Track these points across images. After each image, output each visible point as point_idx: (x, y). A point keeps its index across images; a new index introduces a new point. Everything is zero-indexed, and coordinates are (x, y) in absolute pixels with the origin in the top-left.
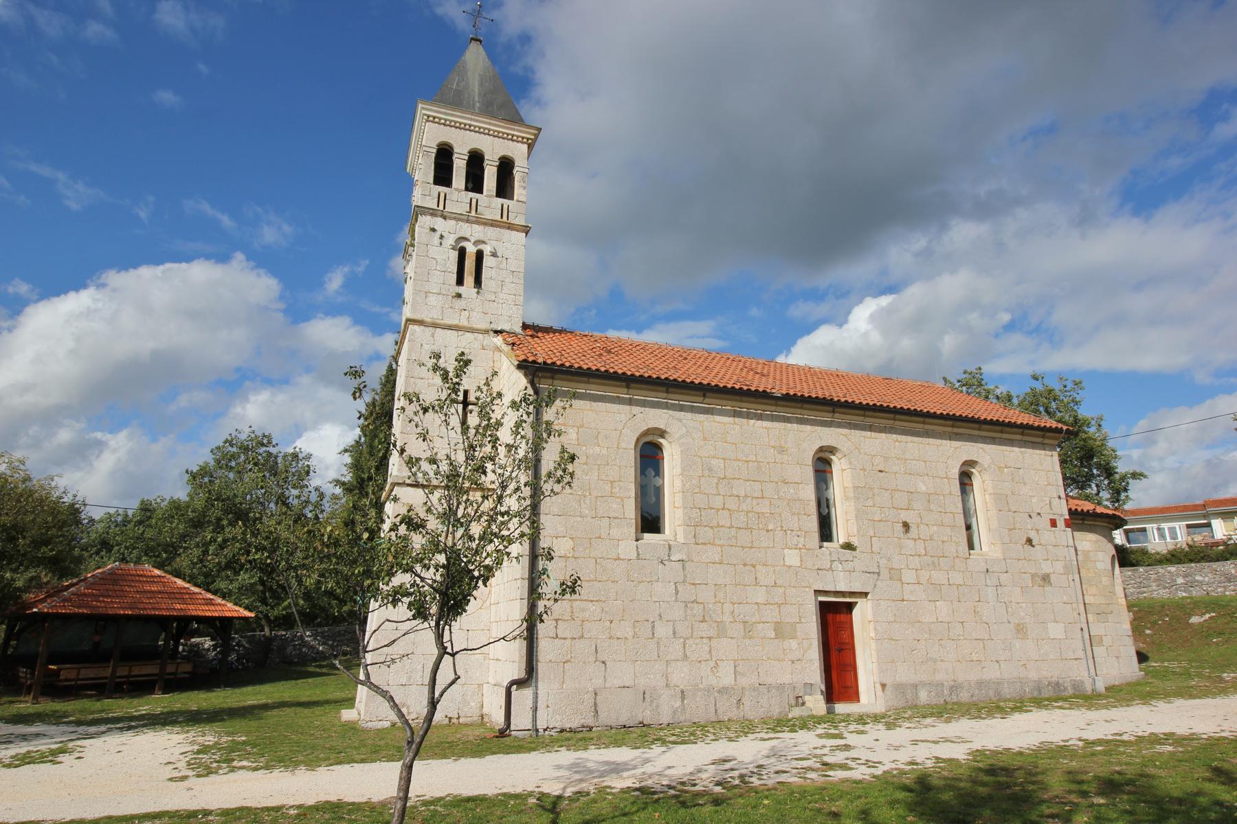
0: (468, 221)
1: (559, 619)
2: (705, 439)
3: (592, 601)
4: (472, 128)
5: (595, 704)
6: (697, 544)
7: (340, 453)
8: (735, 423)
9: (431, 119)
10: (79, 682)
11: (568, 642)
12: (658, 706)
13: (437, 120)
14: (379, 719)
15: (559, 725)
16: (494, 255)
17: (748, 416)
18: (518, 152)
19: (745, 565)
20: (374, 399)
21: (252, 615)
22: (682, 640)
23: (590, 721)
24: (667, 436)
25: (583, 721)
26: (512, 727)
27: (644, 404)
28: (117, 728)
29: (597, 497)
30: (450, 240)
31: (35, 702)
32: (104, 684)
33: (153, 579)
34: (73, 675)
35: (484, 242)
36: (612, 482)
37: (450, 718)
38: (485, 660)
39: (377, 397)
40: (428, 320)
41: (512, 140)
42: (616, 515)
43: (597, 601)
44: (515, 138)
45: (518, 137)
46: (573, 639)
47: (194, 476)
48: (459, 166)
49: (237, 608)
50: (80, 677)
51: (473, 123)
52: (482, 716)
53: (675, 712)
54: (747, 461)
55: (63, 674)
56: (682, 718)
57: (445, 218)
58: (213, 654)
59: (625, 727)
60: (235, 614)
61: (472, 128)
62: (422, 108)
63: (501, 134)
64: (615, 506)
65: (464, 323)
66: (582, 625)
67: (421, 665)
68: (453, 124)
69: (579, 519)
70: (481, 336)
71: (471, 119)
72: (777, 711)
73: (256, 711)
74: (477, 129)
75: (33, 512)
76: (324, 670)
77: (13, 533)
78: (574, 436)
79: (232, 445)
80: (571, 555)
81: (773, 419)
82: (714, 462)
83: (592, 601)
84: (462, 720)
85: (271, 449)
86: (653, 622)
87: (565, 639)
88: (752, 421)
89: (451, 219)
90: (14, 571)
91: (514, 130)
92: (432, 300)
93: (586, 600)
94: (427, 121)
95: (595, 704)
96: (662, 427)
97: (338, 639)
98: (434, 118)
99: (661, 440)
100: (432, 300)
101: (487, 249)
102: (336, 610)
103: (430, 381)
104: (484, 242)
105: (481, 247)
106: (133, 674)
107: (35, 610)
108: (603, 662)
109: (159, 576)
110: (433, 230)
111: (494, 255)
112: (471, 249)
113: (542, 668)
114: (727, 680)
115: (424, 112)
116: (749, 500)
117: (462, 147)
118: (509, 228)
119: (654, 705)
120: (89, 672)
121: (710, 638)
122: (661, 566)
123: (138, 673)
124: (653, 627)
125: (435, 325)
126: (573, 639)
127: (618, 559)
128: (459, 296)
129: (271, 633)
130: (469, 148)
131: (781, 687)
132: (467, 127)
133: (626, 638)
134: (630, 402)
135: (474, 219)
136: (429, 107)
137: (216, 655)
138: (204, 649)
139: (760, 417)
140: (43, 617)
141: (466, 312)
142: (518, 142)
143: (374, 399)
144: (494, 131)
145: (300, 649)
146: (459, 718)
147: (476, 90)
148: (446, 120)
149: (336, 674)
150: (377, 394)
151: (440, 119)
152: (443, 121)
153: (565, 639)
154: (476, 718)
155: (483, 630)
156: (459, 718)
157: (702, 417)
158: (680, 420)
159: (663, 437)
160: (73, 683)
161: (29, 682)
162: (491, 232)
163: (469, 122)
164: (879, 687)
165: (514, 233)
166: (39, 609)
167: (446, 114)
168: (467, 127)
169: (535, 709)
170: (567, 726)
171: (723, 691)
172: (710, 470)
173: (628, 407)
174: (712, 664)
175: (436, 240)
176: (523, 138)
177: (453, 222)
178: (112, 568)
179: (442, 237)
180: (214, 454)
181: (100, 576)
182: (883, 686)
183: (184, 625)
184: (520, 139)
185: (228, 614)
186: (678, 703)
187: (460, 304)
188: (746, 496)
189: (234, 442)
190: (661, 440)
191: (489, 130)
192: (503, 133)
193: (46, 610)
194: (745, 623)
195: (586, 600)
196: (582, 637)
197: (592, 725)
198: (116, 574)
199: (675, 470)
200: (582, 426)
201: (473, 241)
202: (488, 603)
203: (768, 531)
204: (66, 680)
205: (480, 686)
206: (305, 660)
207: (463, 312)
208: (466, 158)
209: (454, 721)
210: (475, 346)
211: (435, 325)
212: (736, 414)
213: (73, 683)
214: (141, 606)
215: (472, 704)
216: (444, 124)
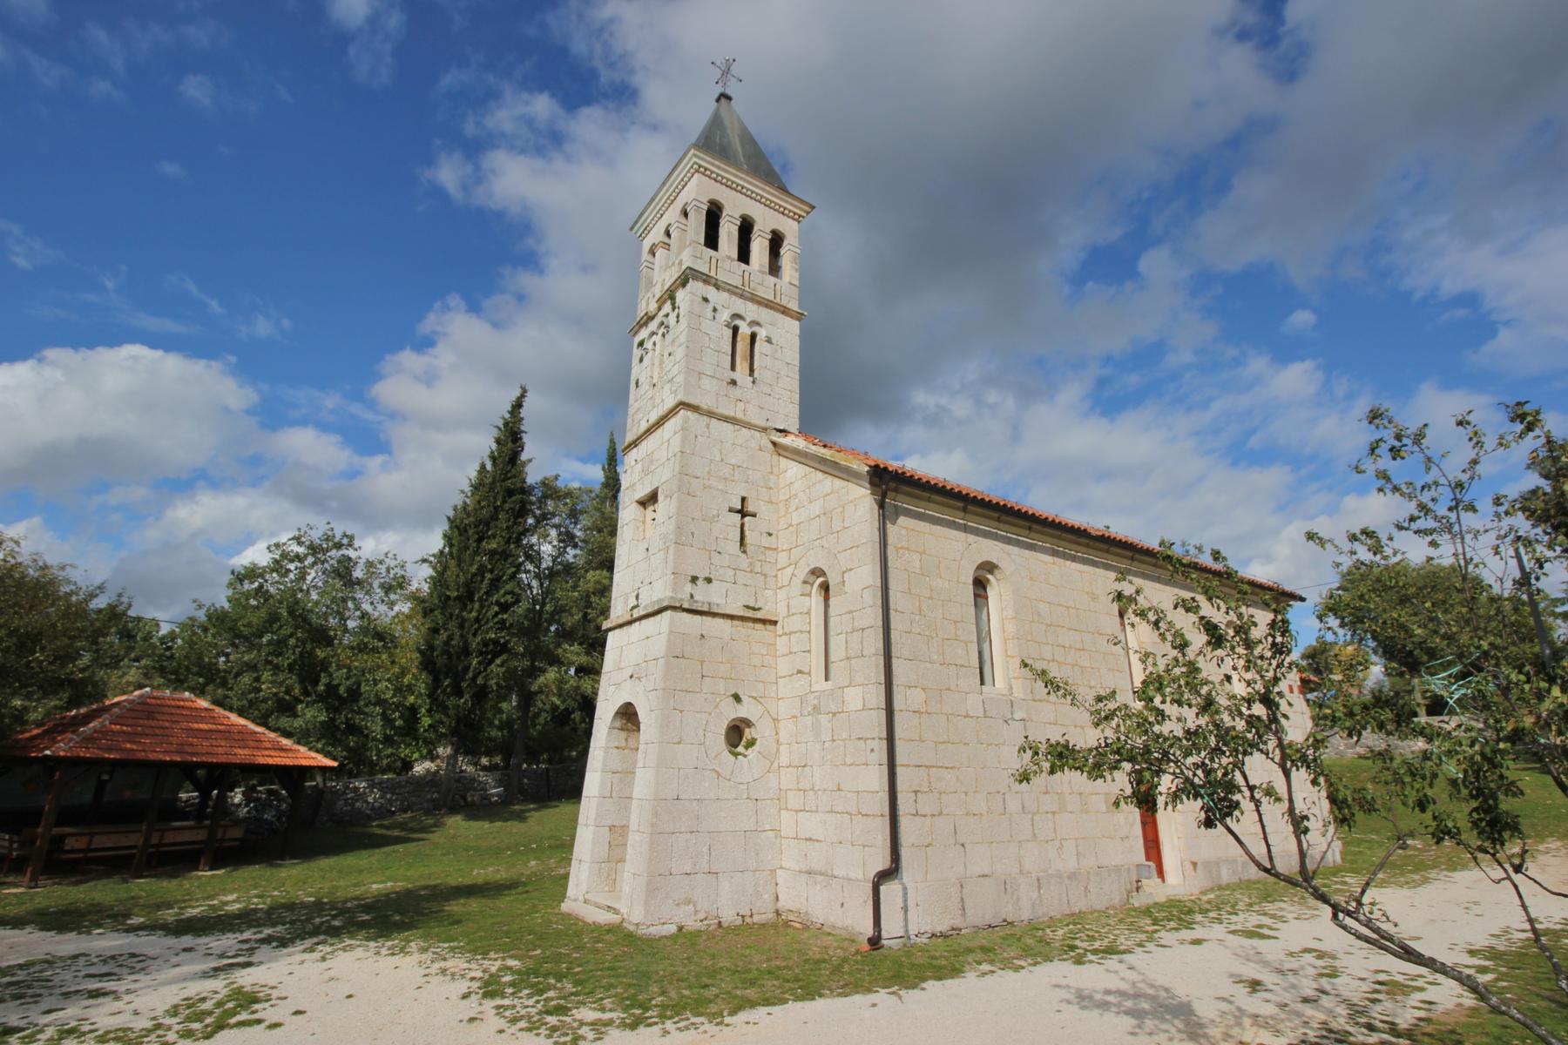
0: (741, 296)
1: (919, 791)
2: (1031, 579)
3: (947, 768)
4: (744, 190)
5: (962, 899)
6: (1034, 700)
7: (416, 562)
8: (1054, 563)
9: (702, 169)
10: (90, 854)
11: (928, 819)
12: (1018, 899)
13: (708, 173)
14: (662, 921)
15: (929, 928)
16: (769, 341)
17: (1064, 556)
18: (789, 228)
19: (1076, 726)
20: (465, 503)
21: (335, 764)
22: (1030, 816)
23: (958, 922)
24: (996, 572)
25: (952, 921)
26: (884, 934)
27: (977, 532)
28: (267, 941)
29: (943, 639)
30: (725, 316)
31: (33, 884)
32: (132, 857)
33: (197, 714)
34: (81, 843)
35: (758, 324)
36: (956, 622)
37: (743, 916)
38: (776, 838)
39: (468, 501)
40: (704, 406)
41: (783, 213)
42: (962, 663)
43: (952, 768)
44: (786, 212)
45: (790, 211)
46: (933, 815)
47: (1344, 576)
48: (728, 232)
49: (313, 754)
50: (93, 847)
51: (746, 185)
52: (778, 913)
53: (1033, 905)
54: (1068, 608)
55: (70, 843)
56: (1040, 913)
57: (718, 289)
58: (246, 809)
59: (990, 926)
60: (313, 763)
61: (744, 190)
62: (695, 155)
63: (773, 205)
64: (960, 651)
65: (740, 415)
66: (939, 799)
67: (707, 847)
68: (724, 181)
69: (928, 665)
70: (758, 434)
71: (745, 180)
72: (1118, 898)
73: (455, 907)
74: (749, 193)
75: (1516, 632)
76: (396, 833)
77: (26, 642)
78: (918, 564)
79: (300, 543)
80: (924, 710)
81: (1085, 561)
82: (1042, 606)
83: (947, 768)
84: (756, 918)
85: (352, 553)
86: (1004, 794)
87: (925, 816)
88: (1068, 563)
89: (725, 290)
90: (28, 697)
91: (787, 202)
92: (706, 383)
93: (941, 767)
94: (697, 171)
95: (962, 899)
96: (994, 561)
97: (397, 791)
98: (706, 169)
99: (989, 576)
100: (706, 383)
101: (762, 333)
102: (374, 753)
103: (706, 482)
104: (758, 324)
105: (756, 329)
106: (166, 841)
107: (48, 752)
108: (963, 845)
109: (206, 709)
110: (706, 300)
111: (769, 341)
112: (745, 330)
113: (905, 853)
114: (1072, 864)
115: (694, 159)
116: (1073, 651)
117: (735, 207)
118: (783, 313)
119: (1015, 897)
120: (106, 840)
121: (1054, 813)
122: (1005, 725)
123: (172, 841)
124: (1004, 800)
125: (710, 414)
126: (933, 815)
127: (967, 716)
128: (734, 382)
129: (325, 784)
130: (741, 213)
131: (1118, 869)
132: (739, 188)
133: (981, 814)
134: (965, 529)
135: (749, 295)
136: (702, 155)
137: (248, 812)
138: (234, 805)
139: (1074, 559)
140: (56, 761)
141: (742, 404)
142: (788, 217)
143: (465, 503)
144: (767, 199)
145: (352, 805)
146: (751, 916)
147: (741, 153)
148: (718, 175)
149: (1269, 937)
150: (467, 497)
151: (712, 172)
152: (714, 176)
153: (925, 816)
154: (771, 916)
155: (772, 799)
156: (751, 916)
157: (1027, 553)
158: (1009, 555)
159: (991, 572)
160: (81, 855)
161: (15, 853)
162: (764, 314)
163: (742, 183)
164: (1188, 866)
165: (788, 319)
166: (53, 752)
167: (719, 168)
168: (739, 188)
169: (905, 909)
170: (938, 929)
171: (1072, 876)
172: (1039, 614)
173: (963, 534)
174: (1057, 843)
175: (710, 314)
176: (795, 214)
177: (726, 295)
178: (141, 696)
179: (715, 310)
180: (270, 551)
181: (128, 706)
182: (1195, 864)
183: (222, 775)
184: (791, 214)
185: (305, 763)
186: (1036, 893)
187: (735, 392)
188: (1070, 647)
189: (303, 539)
190: (989, 576)
191: (762, 197)
192: (776, 204)
193: (62, 754)
194: (1081, 794)
195: (941, 767)
196: (940, 814)
197: (960, 926)
198: (148, 704)
199: (1005, 613)
200: (924, 552)
201: (748, 320)
202: (776, 765)
203: (1091, 688)
204: (72, 851)
205: (773, 872)
206: (362, 818)
207: (739, 403)
208: (739, 223)
209: (748, 920)
210: (753, 445)
211: (710, 414)
212: (1055, 553)
213: (81, 855)
214: (189, 749)
215: (766, 896)
216: (715, 180)
